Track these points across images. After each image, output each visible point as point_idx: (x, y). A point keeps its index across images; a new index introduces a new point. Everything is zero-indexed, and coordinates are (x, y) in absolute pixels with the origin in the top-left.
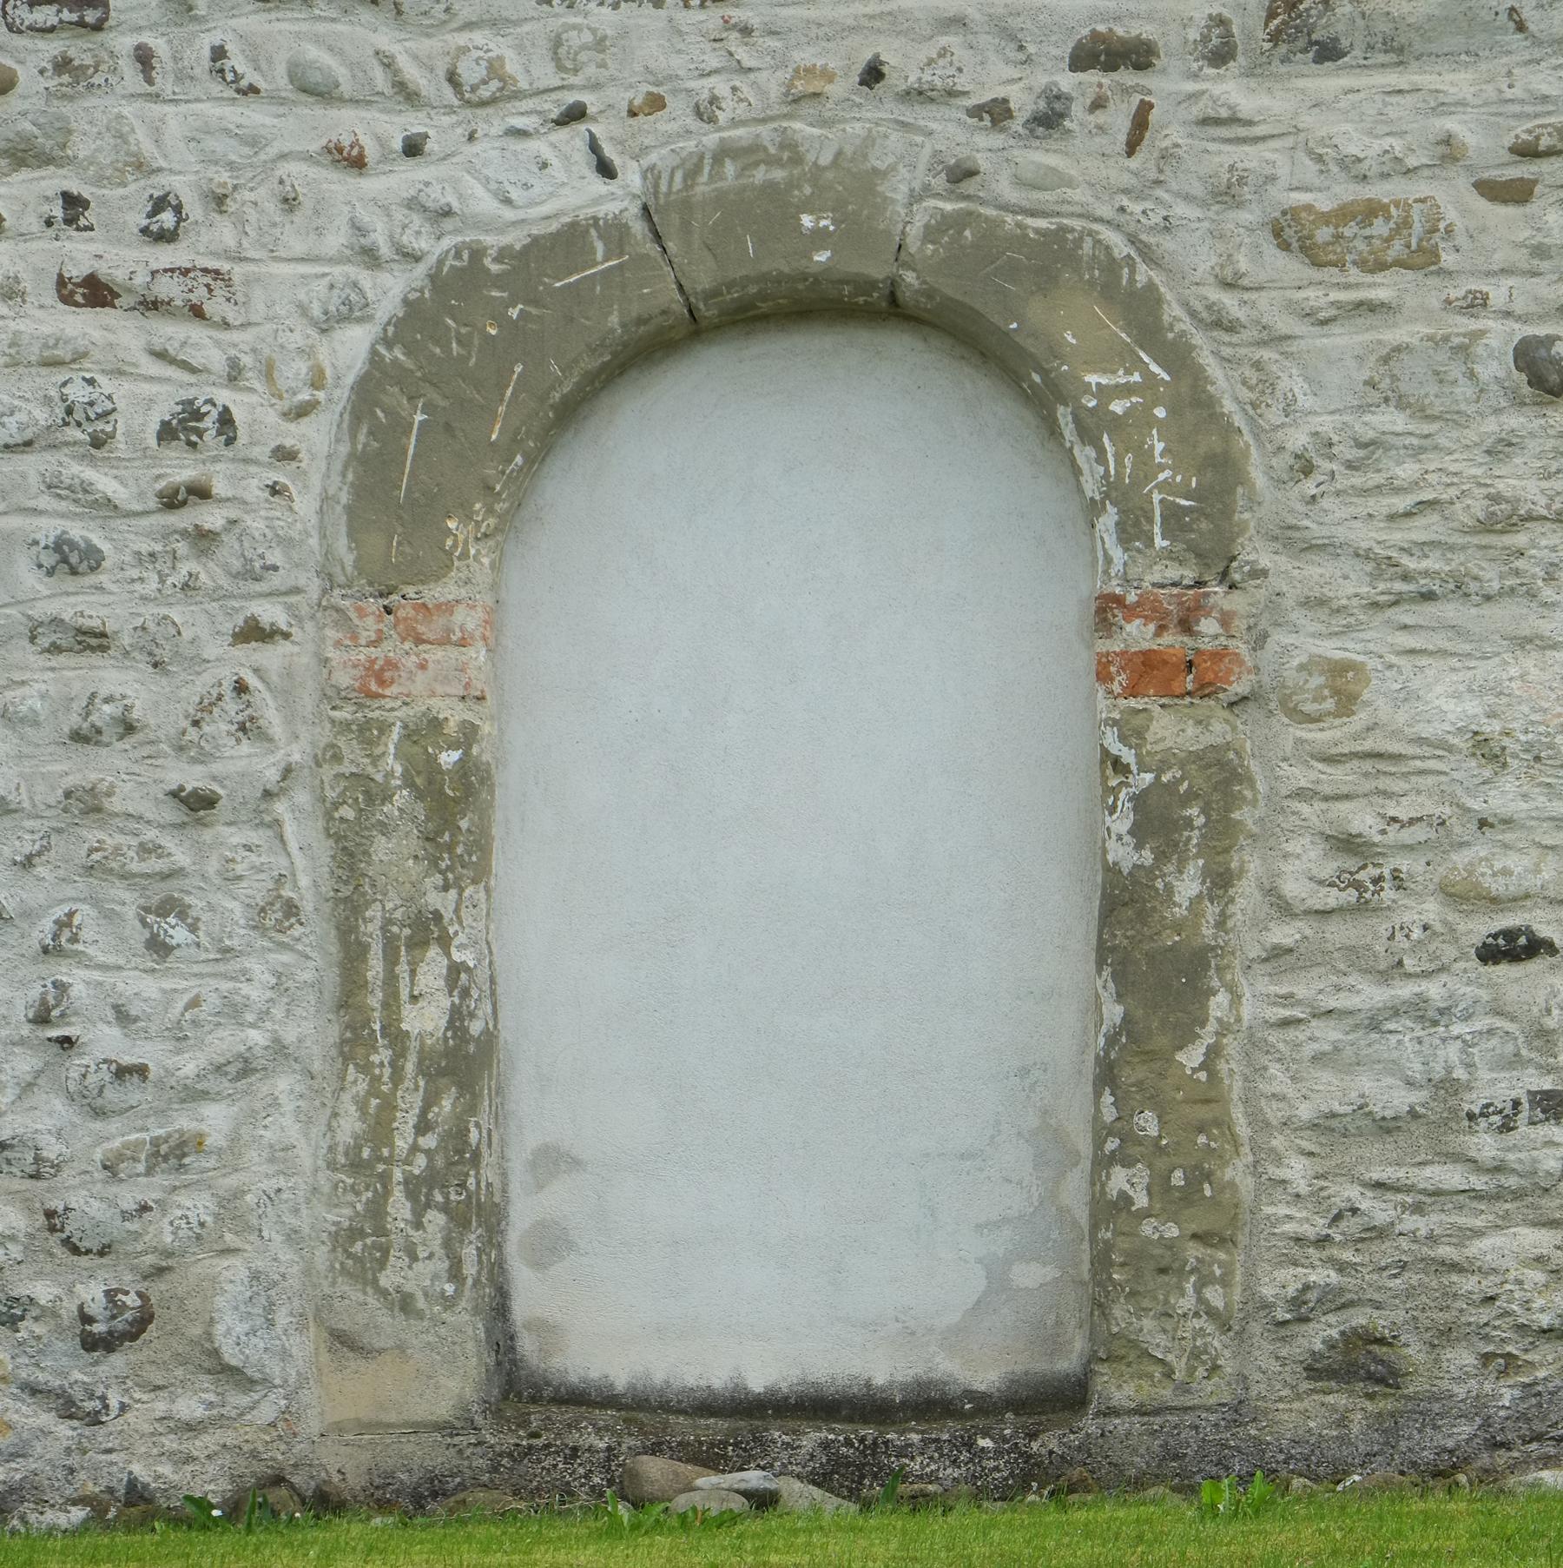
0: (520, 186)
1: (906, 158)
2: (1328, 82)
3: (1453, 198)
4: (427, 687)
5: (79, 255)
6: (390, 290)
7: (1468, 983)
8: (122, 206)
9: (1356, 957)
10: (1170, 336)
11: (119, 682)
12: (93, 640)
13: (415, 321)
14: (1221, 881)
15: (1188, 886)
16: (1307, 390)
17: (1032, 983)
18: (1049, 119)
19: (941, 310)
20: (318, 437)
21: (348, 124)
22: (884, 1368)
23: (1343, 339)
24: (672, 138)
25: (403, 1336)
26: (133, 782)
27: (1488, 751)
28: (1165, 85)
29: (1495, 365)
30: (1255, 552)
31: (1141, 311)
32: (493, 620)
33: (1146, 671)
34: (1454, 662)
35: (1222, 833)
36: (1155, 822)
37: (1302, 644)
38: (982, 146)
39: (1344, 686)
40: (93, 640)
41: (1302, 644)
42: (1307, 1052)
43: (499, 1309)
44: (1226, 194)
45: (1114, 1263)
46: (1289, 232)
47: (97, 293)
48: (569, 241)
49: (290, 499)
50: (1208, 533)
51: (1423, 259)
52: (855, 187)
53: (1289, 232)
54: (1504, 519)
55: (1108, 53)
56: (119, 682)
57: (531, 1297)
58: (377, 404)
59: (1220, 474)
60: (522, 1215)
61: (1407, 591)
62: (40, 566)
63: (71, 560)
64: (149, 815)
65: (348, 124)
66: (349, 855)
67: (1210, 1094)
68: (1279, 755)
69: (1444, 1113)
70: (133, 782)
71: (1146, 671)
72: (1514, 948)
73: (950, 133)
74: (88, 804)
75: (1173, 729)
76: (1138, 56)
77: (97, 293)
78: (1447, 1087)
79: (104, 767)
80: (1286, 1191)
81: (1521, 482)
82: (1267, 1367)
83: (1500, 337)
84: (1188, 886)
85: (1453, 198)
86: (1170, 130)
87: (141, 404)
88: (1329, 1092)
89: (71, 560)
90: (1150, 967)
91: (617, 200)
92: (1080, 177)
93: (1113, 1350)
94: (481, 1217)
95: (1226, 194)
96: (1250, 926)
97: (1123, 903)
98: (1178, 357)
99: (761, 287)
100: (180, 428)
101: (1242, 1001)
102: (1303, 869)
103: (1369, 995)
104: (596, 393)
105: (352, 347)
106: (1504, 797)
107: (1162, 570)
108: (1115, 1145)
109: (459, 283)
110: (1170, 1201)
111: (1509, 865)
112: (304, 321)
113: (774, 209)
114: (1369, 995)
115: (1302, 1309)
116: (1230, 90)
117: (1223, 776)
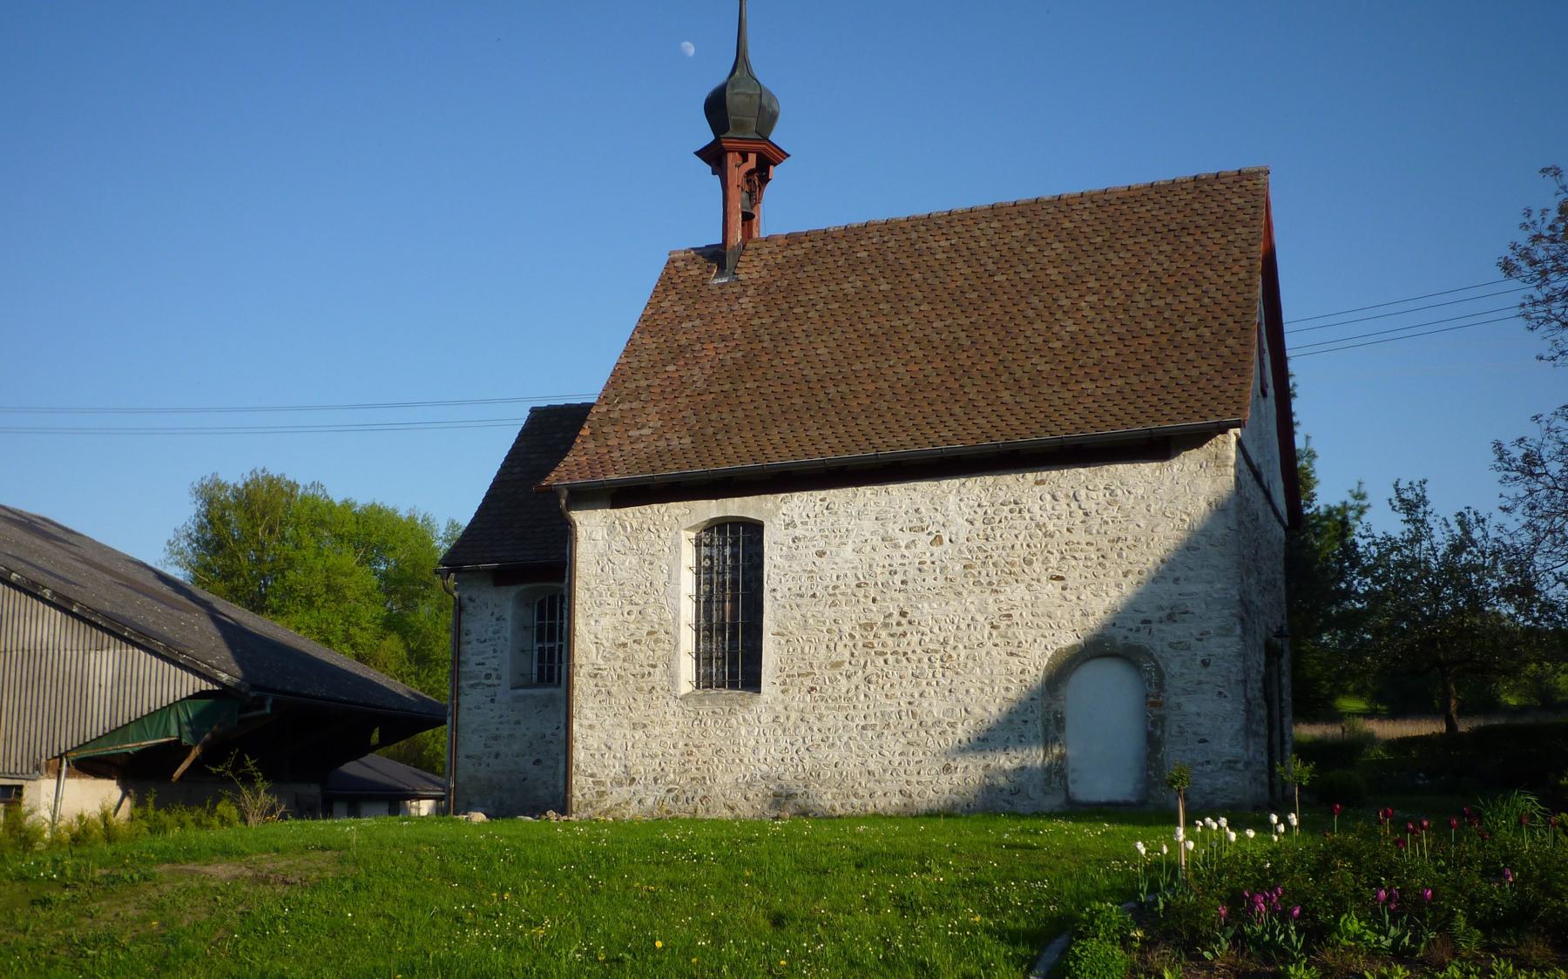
3: (1193, 641)
4: (1055, 706)
5: (1009, 649)
10: (1274, 818)
15: (1159, 732)
16: (1174, 667)
18: (1138, 630)
22: (1119, 798)
25: (769, 932)
31: (1151, 656)
33: (1153, 704)
36: (1154, 724)
37: (1174, 700)
39: (1179, 705)
41: (1174, 700)
42: (1175, 756)
43: (1067, 790)
46: (1171, 645)
47: (1012, 654)
50: (1160, 686)
53: (1171, 645)
54: (1200, 683)
55: (1145, 622)
57: (1072, 788)
60: (1070, 777)
61: (1186, 692)
64: (1361, 720)
66: (1046, 729)
71: (1153, 704)
72: (1203, 741)
73: (1124, 632)
75: (1156, 712)
76: (1149, 622)
81: (1202, 678)
83: (1199, 659)
84: (1159, 732)
85: (1193, 641)
92: (1142, 639)
94: (1065, 777)
102: (1174, 730)
106: (1201, 720)
107: (1154, 690)
116: (1163, 627)
117: (1162, 719)
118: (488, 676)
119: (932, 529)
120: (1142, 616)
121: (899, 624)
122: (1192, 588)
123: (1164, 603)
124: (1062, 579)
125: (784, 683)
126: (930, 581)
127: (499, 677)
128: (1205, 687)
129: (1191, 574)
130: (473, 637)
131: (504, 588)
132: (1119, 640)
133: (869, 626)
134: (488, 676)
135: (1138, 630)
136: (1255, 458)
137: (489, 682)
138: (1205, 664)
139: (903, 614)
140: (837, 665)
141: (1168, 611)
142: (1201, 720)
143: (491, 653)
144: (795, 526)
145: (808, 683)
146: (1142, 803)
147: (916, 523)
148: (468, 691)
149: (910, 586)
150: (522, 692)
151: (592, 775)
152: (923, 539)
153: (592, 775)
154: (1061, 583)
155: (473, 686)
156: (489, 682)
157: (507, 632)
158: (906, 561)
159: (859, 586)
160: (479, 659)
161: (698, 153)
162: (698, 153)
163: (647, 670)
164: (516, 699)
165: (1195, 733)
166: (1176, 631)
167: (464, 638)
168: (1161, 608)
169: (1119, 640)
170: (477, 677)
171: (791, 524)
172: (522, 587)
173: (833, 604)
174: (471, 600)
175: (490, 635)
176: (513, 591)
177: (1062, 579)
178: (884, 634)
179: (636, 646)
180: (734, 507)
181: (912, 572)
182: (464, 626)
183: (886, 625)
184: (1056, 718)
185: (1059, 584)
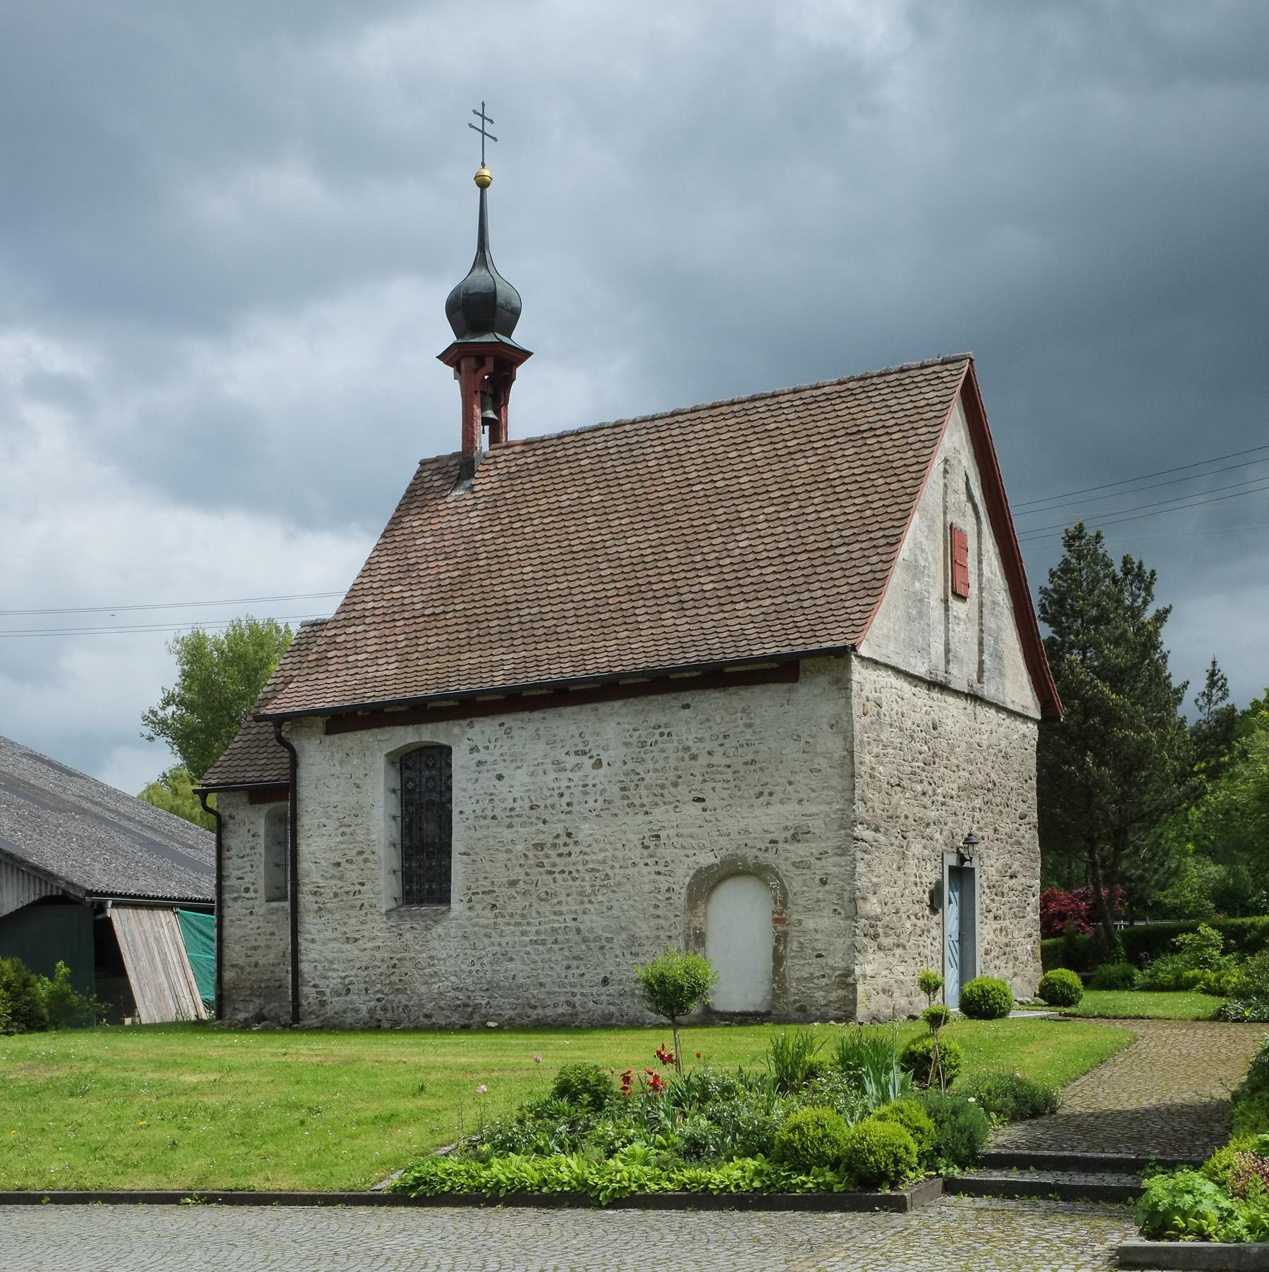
0: (707, 859)
1: (750, 855)
2: (799, 845)
3: (813, 860)
5: (658, 868)
6: (692, 872)
7: (815, 960)
8: (662, 862)
9: (801, 957)
11: (662, 922)
12: (659, 917)
13: (695, 876)
14: (785, 947)
16: (795, 886)
17: (764, 961)
18: (767, 850)
19: (759, 872)
20: (684, 891)
21: (687, 852)
22: (751, 1009)
23: (800, 878)
24: (724, 853)
26: (663, 935)
27: (816, 931)
28: (780, 845)
29: (817, 881)
30: (789, 905)
31: (777, 874)
32: (705, 914)
34: (167, 863)
35: (785, 941)
36: (777, 940)
37: (795, 917)
38: (759, 854)
39: (800, 922)
40: (659, 917)
41: (795, 917)
42: (796, 969)
44: (786, 859)
45: (776, 997)
46: (794, 864)
47: (659, 873)
48: (711, 866)
49: (680, 899)
50: (784, 903)
51: (809, 868)
52: (744, 859)
53: (794, 864)
54: (818, 901)
55: (773, 842)
56: (662, 922)
58: (854, 823)
59: (785, 895)
61: (808, 910)
62: (151, 739)
63: (656, 907)
65: (687, 852)
67: (784, 975)
68: (793, 931)
69: (811, 978)
70: (663, 935)
72: (819, 956)
73: (755, 851)
74: (658, 937)
75: (780, 928)
77: (659, 873)
78: (812, 974)
79: (660, 933)
80: (793, 987)
81: (820, 896)
82: (791, 1009)
83: (818, 877)
85: (813, 860)
86: (780, 851)
87: (664, 887)
88: (798, 975)
89: (656, 907)
90: (778, 959)
91: (717, 861)
92: (769, 858)
93: (774, 1007)
95: (786, 859)
96: (789, 953)
97: (775, 950)
98: (780, 880)
99: (732, 870)
100: (668, 890)
101: (788, 963)
102: (795, 946)
103: (803, 962)
104: (176, 1031)
105: (688, 880)
106: (818, 937)
108: (774, 981)
109: (699, 871)
110: (779, 988)
111: (819, 946)
112: (682, 877)
113: (734, 862)
114: (803, 962)
115: (795, 1001)
116: (787, 846)
117: (786, 934)
118: (247, 890)
119: (594, 753)
120: (770, 837)
121: (565, 845)
122: (814, 809)
123: (789, 824)
124: (703, 800)
125: (470, 901)
126: (591, 804)
127: (256, 891)
128: (823, 904)
129: (813, 795)
130: (233, 852)
131: (258, 806)
132: (751, 861)
133: (540, 846)
134: (247, 890)
135: (767, 850)
136: (921, 670)
137: (248, 895)
138: (823, 882)
139: (569, 835)
140: (513, 883)
141: (792, 831)
142: (201, 1061)
143: (249, 868)
144: (478, 751)
145: (489, 899)
146: (768, 1013)
147: (581, 747)
148: (230, 903)
149: (575, 808)
150: (274, 904)
151: (315, 986)
152: (588, 763)
153: (315, 986)
154: (701, 805)
155: (235, 899)
156: (248, 895)
157: (261, 849)
158: (571, 784)
159: (532, 808)
160: (239, 873)
161: (527, 354)
162: (527, 354)
163: (358, 887)
164: (272, 912)
165: (814, 949)
166: (800, 850)
167: (226, 854)
168: (786, 828)
169: (751, 861)
170: (238, 891)
171: (474, 749)
172: (273, 805)
173: (510, 826)
174: (232, 817)
175: (248, 851)
176: (265, 808)
177: (703, 800)
178: (553, 853)
179: (348, 866)
180: (428, 734)
181: (577, 792)
182: (226, 842)
183: (554, 846)
184: (695, 934)
185: (700, 805)
